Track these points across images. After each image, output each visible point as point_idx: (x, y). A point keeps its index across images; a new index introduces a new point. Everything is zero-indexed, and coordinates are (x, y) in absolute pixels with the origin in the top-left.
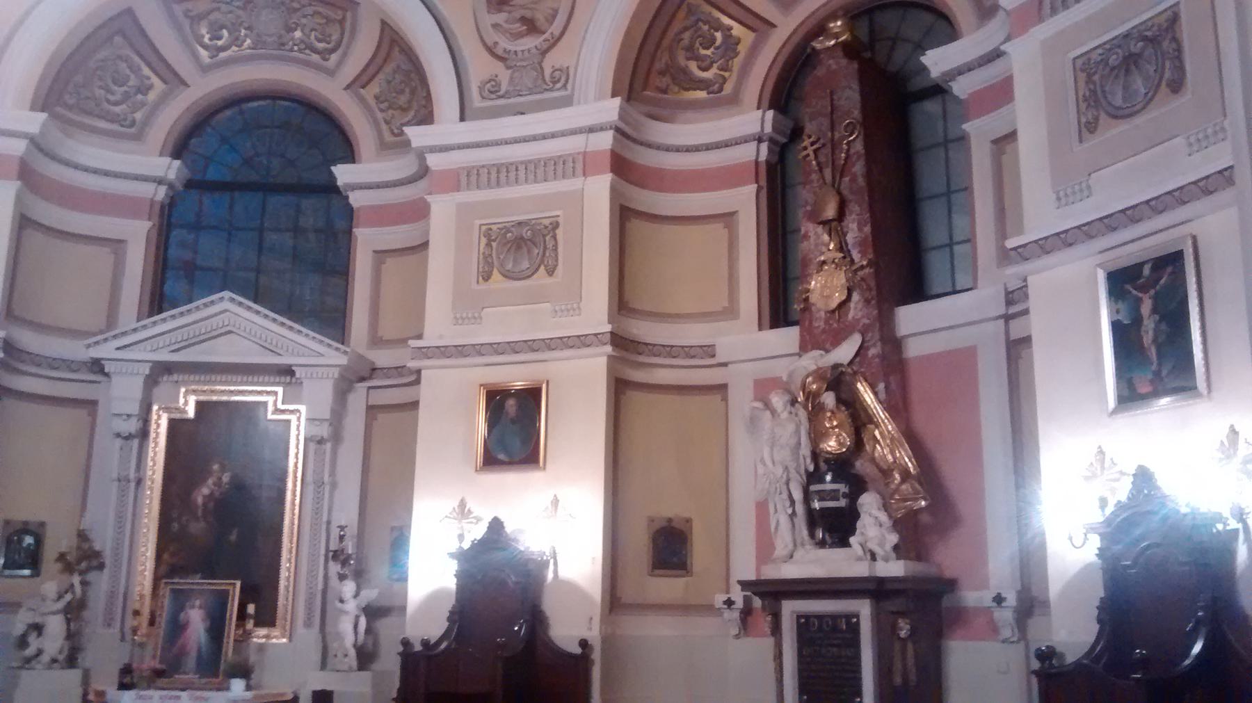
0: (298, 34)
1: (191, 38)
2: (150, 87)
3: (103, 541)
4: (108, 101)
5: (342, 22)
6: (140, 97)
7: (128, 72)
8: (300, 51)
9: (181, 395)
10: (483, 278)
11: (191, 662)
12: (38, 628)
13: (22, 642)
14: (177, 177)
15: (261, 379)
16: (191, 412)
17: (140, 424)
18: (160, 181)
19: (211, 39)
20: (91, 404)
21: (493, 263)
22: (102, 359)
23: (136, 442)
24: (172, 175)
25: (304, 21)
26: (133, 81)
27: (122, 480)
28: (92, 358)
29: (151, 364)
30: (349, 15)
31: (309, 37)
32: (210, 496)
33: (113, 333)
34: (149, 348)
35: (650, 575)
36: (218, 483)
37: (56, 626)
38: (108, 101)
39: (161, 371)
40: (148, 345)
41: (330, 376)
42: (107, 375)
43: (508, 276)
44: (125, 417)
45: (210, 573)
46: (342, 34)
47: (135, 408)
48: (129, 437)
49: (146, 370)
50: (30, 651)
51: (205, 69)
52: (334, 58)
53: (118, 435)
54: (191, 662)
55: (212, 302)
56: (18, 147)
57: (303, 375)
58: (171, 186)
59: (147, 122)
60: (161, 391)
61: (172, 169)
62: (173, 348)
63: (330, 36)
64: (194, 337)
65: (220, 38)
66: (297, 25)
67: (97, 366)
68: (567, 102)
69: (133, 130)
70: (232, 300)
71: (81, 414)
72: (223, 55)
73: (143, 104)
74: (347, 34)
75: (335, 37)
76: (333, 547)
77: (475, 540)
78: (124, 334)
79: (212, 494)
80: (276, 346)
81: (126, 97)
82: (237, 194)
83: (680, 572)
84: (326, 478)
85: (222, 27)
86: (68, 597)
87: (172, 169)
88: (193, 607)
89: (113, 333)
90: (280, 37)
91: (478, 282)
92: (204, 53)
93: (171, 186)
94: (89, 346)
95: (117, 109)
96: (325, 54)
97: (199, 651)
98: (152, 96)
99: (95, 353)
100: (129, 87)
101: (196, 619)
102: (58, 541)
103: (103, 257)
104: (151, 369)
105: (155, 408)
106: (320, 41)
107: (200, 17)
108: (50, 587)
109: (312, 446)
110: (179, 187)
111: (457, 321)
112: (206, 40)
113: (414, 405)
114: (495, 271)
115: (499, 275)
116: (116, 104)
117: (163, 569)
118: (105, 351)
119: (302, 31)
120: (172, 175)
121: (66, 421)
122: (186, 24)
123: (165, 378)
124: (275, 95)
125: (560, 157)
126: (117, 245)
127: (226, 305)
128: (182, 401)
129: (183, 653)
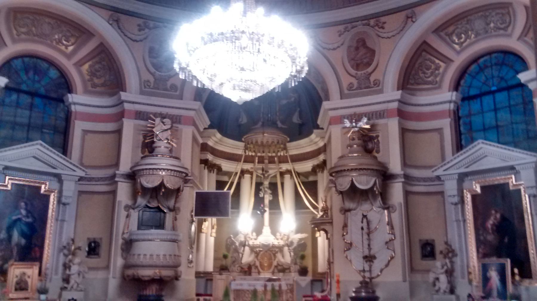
0: (492, 25)
1: (450, 42)
2: (440, 67)
3: (456, 246)
4: (426, 77)
5: (509, 13)
6: (437, 72)
7: (430, 64)
8: (495, 31)
9: (474, 185)
11: (495, 293)
12: (437, 279)
13: (434, 285)
14: (456, 98)
16: (479, 190)
17: (459, 198)
18: (450, 102)
19: (458, 40)
20: (442, 193)
22: (515, 165)
23: (459, 206)
24: (454, 98)
25: (493, 19)
26: (433, 67)
27: (458, 221)
28: (436, 176)
30: (510, 9)
31: (497, 24)
32: (494, 225)
33: (444, 163)
34: (456, 168)
36: (495, 218)
37: (443, 278)
38: (426, 77)
39: (462, 178)
40: (455, 167)
42: (443, 181)
44: (453, 197)
45: (499, 256)
46: (510, 17)
47: (455, 192)
48: (456, 204)
49: (456, 177)
50: (437, 288)
51: (458, 53)
52: (510, 29)
53: (452, 204)
54: (495, 293)
55: (475, 146)
56: (395, 105)
58: (455, 102)
59: (441, 80)
60: (466, 184)
61: (453, 96)
62: (467, 165)
63: (506, 20)
65: (461, 38)
66: (490, 22)
67: (438, 178)
68: (381, 92)
69: (437, 85)
70: (483, 143)
71: (439, 197)
72: (464, 45)
73: (439, 74)
74: (512, 19)
75: (508, 20)
78: (448, 162)
79: (494, 223)
80: (506, 158)
81: (432, 73)
82: (471, 102)
84: (461, 218)
85: (461, 34)
86: (445, 268)
87: (453, 96)
88: (492, 270)
89: (444, 163)
90: (485, 28)
92: (457, 47)
93: (455, 102)
94: (433, 172)
95: (430, 79)
96: (505, 29)
97: (498, 289)
98: (441, 70)
99: (436, 173)
100: (432, 69)
101: (494, 275)
102: (439, 247)
103: (435, 136)
104: (459, 176)
105: (465, 191)
106: (501, 24)
107: (452, 34)
108: (438, 264)
109: (532, 199)
110: (460, 102)
112: (457, 41)
116: (429, 77)
117: (480, 255)
118: (440, 172)
119: (494, 23)
120: (454, 98)
121: (432, 201)
122: (447, 38)
123: (466, 179)
124: (489, 53)
125: (371, 112)
126: (439, 131)
127: (481, 145)
128: (474, 187)
129: (491, 290)
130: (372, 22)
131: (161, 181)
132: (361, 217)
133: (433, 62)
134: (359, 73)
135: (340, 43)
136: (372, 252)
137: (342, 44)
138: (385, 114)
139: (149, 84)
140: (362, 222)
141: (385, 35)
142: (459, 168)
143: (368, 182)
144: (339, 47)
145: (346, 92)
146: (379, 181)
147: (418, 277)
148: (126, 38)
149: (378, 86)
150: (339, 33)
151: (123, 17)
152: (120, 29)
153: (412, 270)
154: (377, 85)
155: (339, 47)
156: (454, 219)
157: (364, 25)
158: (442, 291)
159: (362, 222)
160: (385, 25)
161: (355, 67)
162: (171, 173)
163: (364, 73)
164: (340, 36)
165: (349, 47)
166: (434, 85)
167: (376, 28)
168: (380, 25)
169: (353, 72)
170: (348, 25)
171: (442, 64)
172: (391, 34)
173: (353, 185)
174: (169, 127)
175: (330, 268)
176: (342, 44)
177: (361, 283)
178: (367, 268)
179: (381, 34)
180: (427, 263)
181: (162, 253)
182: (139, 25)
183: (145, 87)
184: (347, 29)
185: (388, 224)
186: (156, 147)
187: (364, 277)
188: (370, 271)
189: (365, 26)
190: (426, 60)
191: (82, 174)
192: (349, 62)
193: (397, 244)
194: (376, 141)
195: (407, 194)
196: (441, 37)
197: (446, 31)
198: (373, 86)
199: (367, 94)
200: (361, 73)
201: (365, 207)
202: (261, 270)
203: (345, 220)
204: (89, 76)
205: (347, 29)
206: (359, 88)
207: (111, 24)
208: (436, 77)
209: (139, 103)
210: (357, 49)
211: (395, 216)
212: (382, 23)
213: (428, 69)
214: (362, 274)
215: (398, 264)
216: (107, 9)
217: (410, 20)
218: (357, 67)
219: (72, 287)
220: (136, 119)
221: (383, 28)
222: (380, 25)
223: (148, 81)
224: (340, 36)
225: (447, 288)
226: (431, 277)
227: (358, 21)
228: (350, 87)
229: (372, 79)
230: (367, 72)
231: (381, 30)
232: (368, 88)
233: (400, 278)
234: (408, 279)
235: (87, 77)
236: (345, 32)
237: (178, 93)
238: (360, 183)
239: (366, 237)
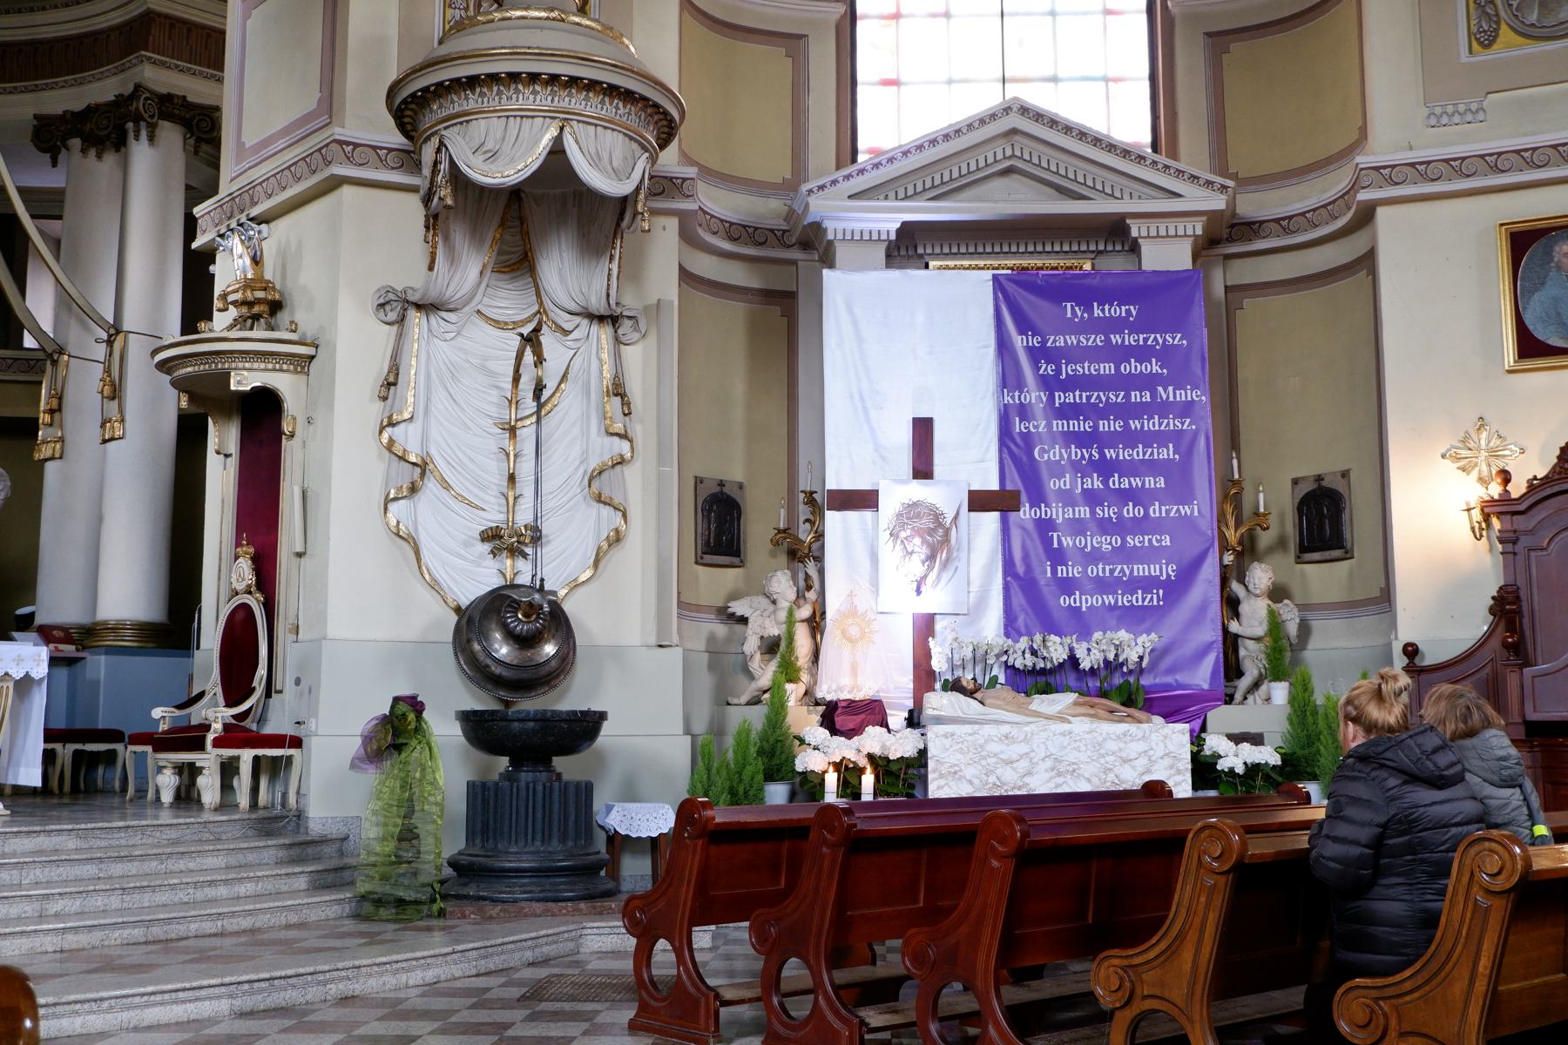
10: (1481, 44)
15: (1110, 248)
21: (1497, 15)
29: (1204, 218)
35: (1298, 563)
41: (1190, 232)
43: (1531, 34)
57: (1144, 233)
64: (933, 187)
76: (811, 568)
77: (1535, 478)
83: (1337, 553)
91: (1471, 52)
111: (1436, 120)
113: (1368, 262)
114: (1504, 27)
115: (1512, 34)
193: (635, 485)
211: (639, 360)
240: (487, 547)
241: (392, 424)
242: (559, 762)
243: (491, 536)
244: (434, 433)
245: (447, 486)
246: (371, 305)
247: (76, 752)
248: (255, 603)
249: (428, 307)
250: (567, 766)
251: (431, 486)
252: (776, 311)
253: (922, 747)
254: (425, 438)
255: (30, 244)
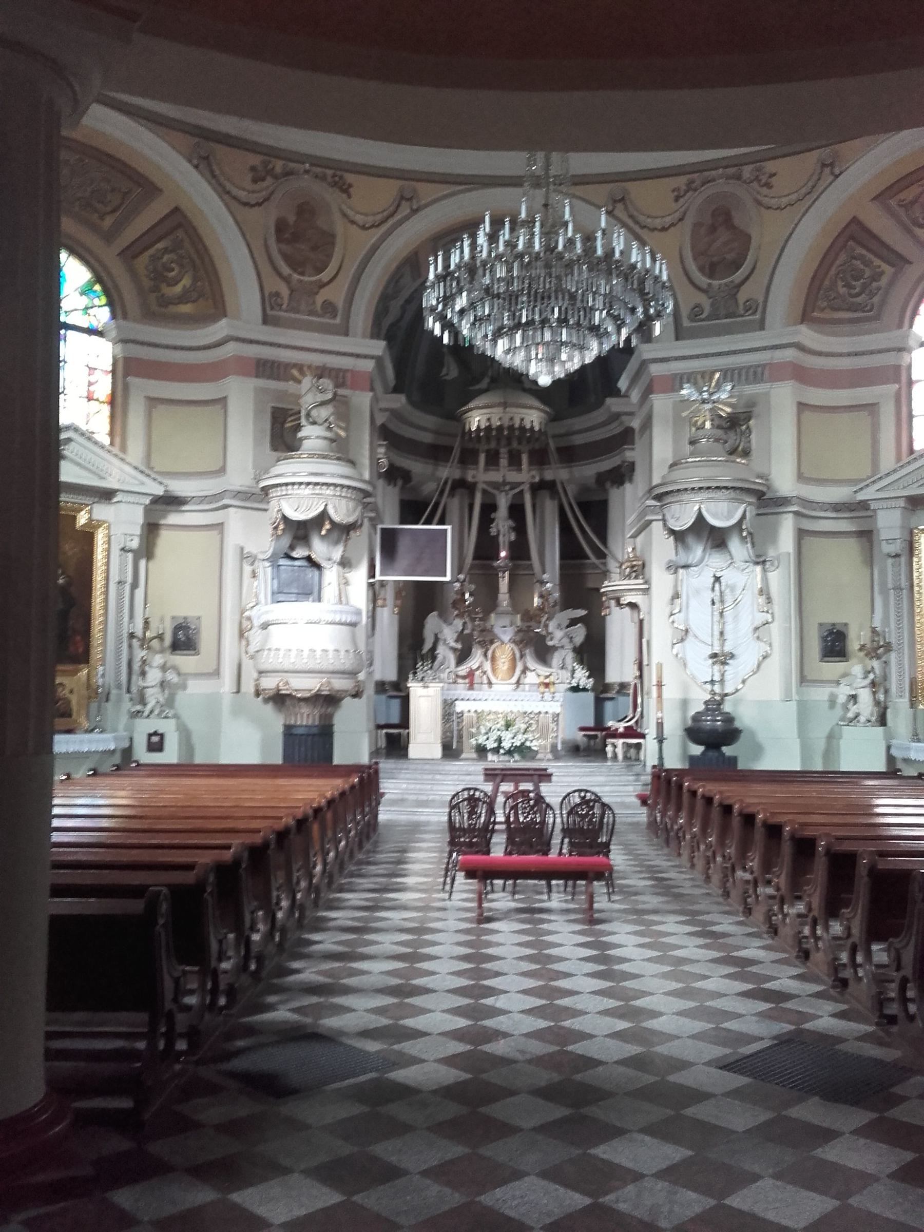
2: (882, 273)
6: (874, 284)
7: (862, 267)
12: (854, 698)
23: (903, 560)
26: (868, 273)
27: (898, 588)
37: (865, 696)
47: (896, 533)
48: (897, 556)
53: (889, 556)
68: (761, 326)
73: (879, 289)
81: (865, 287)
86: (871, 676)
95: (859, 300)
98: (884, 281)
108: (857, 669)
130: (747, 171)
131: (321, 508)
132: (712, 580)
133: (868, 264)
134: (716, 283)
135: (677, 215)
136: (727, 648)
137: (681, 220)
138: (767, 373)
139: (279, 300)
140: (713, 589)
141: (773, 202)
142: (904, 487)
143: (730, 516)
144: (673, 225)
145: (686, 323)
146: (751, 512)
147: (820, 694)
148: (226, 197)
149: (754, 313)
150: (676, 193)
151: (221, 151)
152: (214, 176)
153: (803, 679)
154: (750, 312)
155: (673, 225)
156: (890, 585)
157: (728, 178)
158: (862, 719)
159: (713, 589)
160: (773, 180)
161: (707, 271)
162: (341, 491)
163: (726, 285)
164: (677, 199)
165: (697, 226)
166: (868, 311)
167: (755, 184)
168: (764, 179)
169: (703, 280)
170: (695, 175)
171: (885, 267)
172: (785, 201)
173: (700, 518)
174: (329, 396)
175: (641, 677)
176: (681, 220)
177: (706, 703)
178: (717, 678)
179: (766, 201)
180: (834, 668)
181: (331, 647)
182: (253, 169)
183: (272, 308)
184: (694, 186)
185: (761, 592)
186: (301, 439)
187: (713, 693)
188: (722, 681)
189: (731, 181)
190: (854, 258)
191: (159, 491)
192: (695, 258)
193: (776, 631)
194: (744, 427)
195: (801, 534)
196: (889, 210)
197: (902, 196)
198: (742, 312)
199: (728, 331)
200: (720, 285)
201: (715, 562)
202: (493, 680)
203: (676, 586)
204: (151, 279)
205: (694, 186)
206: (714, 316)
207: (196, 167)
208: (872, 295)
209: (258, 342)
210: (713, 229)
211: (775, 577)
212: (767, 175)
213: (856, 279)
214: (709, 687)
215: (775, 666)
216: (187, 132)
217: (827, 170)
218: (711, 270)
219: (151, 712)
220: (257, 376)
221: (768, 185)
222: (764, 179)
223: (277, 294)
224: (677, 199)
225: (872, 715)
226: (843, 692)
227: (716, 169)
228: (696, 313)
229: (742, 297)
230: (732, 282)
231: (765, 190)
232: (731, 317)
233: (776, 694)
234: (795, 697)
235: (147, 283)
236: (686, 192)
237: (338, 320)
238: (715, 516)
239: (717, 617)
240: (710, 661)
241: (672, 615)
242: (724, 749)
243: (714, 656)
244: (691, 616)
245: (696, 637)
246: (664, 567)
247: (624, 743)
248: (638, 681)
249: (686, 567)
250: (727, 750)
251: (690, 638)
252: (864, 539)
253: (126, 744)
254: (687, 620)
255: (648, 432)
